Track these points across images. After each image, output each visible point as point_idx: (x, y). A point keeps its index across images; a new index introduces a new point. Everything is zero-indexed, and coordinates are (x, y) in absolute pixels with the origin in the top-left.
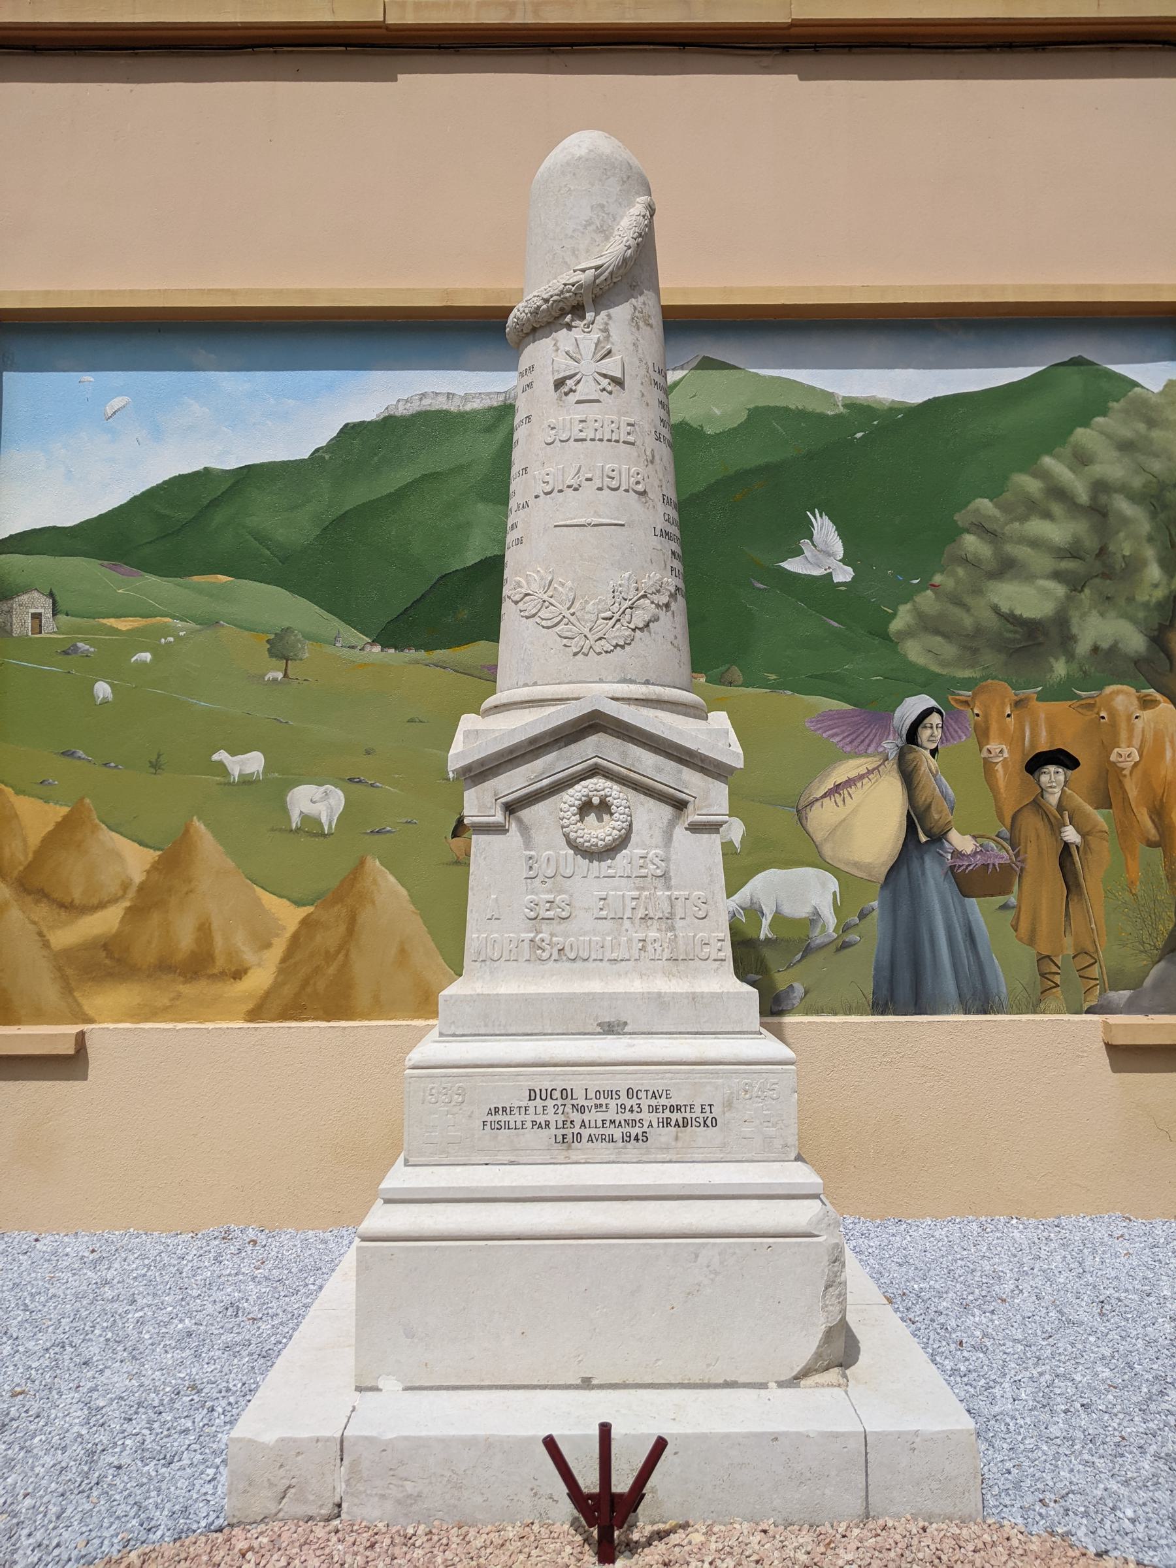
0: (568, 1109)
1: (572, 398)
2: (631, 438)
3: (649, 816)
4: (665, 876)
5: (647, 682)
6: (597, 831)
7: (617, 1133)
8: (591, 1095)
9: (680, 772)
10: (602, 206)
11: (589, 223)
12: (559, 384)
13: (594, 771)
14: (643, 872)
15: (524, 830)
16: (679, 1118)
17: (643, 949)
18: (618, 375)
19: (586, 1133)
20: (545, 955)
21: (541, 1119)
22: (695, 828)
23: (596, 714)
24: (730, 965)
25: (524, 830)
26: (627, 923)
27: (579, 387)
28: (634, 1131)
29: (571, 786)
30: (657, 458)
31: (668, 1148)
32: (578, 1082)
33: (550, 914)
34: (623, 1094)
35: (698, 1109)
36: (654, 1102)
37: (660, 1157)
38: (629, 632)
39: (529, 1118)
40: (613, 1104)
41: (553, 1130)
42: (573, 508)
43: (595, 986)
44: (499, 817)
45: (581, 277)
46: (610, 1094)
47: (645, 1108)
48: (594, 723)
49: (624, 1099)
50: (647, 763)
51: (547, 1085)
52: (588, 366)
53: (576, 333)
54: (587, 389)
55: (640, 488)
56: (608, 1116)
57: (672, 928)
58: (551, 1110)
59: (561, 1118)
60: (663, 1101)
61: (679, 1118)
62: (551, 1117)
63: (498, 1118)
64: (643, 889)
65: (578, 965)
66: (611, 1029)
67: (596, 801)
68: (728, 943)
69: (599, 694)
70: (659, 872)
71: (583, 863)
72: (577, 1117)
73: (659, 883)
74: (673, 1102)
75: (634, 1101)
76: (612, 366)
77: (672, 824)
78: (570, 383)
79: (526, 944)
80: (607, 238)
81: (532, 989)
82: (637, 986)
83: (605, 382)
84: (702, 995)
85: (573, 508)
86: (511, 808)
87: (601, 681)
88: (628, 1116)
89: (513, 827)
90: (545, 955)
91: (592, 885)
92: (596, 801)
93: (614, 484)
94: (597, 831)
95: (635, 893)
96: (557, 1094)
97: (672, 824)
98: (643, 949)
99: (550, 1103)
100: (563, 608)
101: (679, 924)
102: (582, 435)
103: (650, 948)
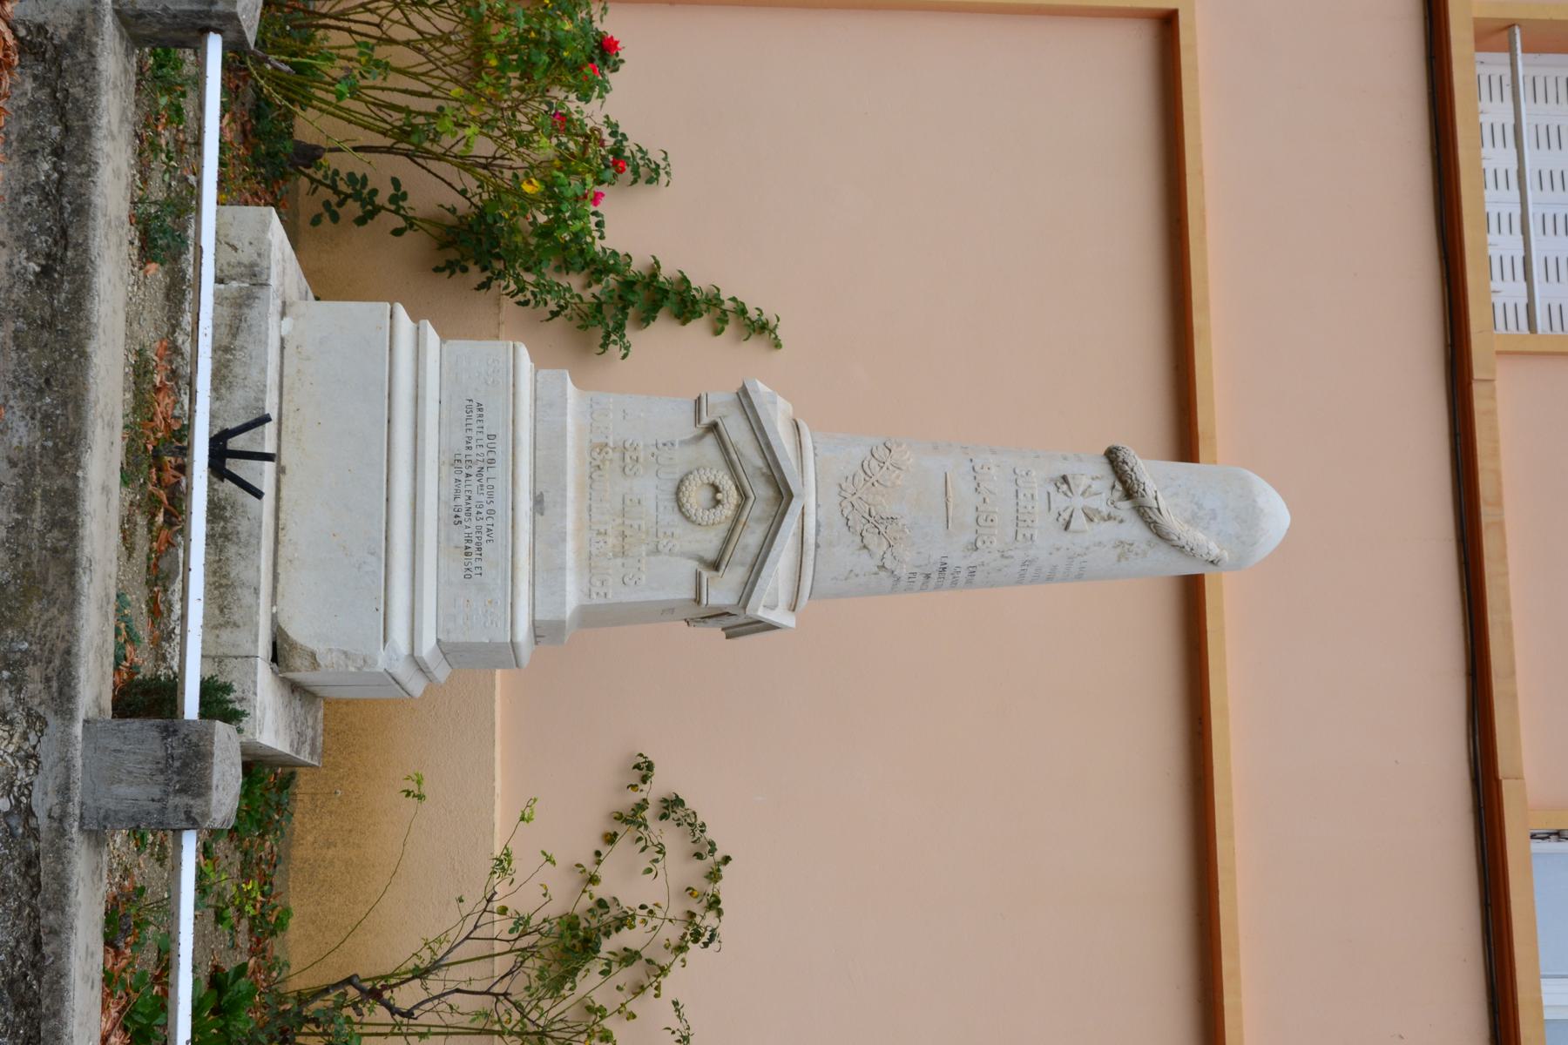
0: (480, 464)
1: (1052, 489)
2: (1020, 537)
3: (708, 543)
4: (657, 551)
5: (817, 546)
6: (696, 497)
7: (462, 501)
8: (491, 482)
9: (743, 564)
10: (1214, 518)
11: (1200, 506)
12: (1065, 479)
13: (744, 496)
14: (661, 534)
15: (699, 438)
16: (471, 550)
17: (599, 533)
18: (1072, 526)
19: (463, 478)
20: (595, 454)
21: (473, 444)
22: (698, 576)
23: (791, 496)
24: (586, 602)
25: (699, 438)
26: (619, 521)
27: (1061, 496)
28: (462, 514)
29: (732, 477)
30: (1006, 562)
31: (448, 539)
32: (500, 472)
33: (628, 460)
34: (491, 507)
35: (478, 564)
36: (484, 530)
37: (443, 535)
38: (859, 530)
39: (473, 434)
40: (484, 498)
41: (465, 452)
42: (962, 487)
43: (571, 493)
44: (706, 420)
45: (1150, 493)
46: (490, 496)
47: (480, 523)
48: (783, 494)
49: (487, 507)
50: (751, 538)
51: (499, 449)
52: (1078, 502)
53: (1106, 494)
54: (1059, 501)
55: (979, 544)
56: (474, 496)
57: (615, 556)
58: (480, 451)
59: (473, 458)
60: (485, 537)
61: (471, 550)
62: (474, 451)
63: (475, 409)
64: (647, 533)
65: (588, 481)
66: (538, 502)
67: (719, 496)
68: (602, 601)
69: (808, 496)
70: (660, 547)
71: (678, 476)
72: (474, 471)
73: (652, 547)
74: (485, 546)
75: (484, 515)
76: (1079, 522)
77: (701, 560)
78: (1065, 487)
79: (603, 440)
80: (1187, 522)
81: (570, 443)
82: (570, 526)
83: (1066, 516)
84: (564, 575)
85: (962, 487)
86: (713, 428)
87: (818, 506)
88: (474, 511)
89: (698, 431)
90: (595, 454)
91: (650, 491)
92: (719, 496)
93: (981, 521)
94: (696, 497)
95: (643, 527)
96: (491, 456)
97: (701, 560)
98: (599, 533)
99: (485, 450)
100: (878, 476)
101: (619, 561)
102: (1021, 496)
103: (600, 538)
